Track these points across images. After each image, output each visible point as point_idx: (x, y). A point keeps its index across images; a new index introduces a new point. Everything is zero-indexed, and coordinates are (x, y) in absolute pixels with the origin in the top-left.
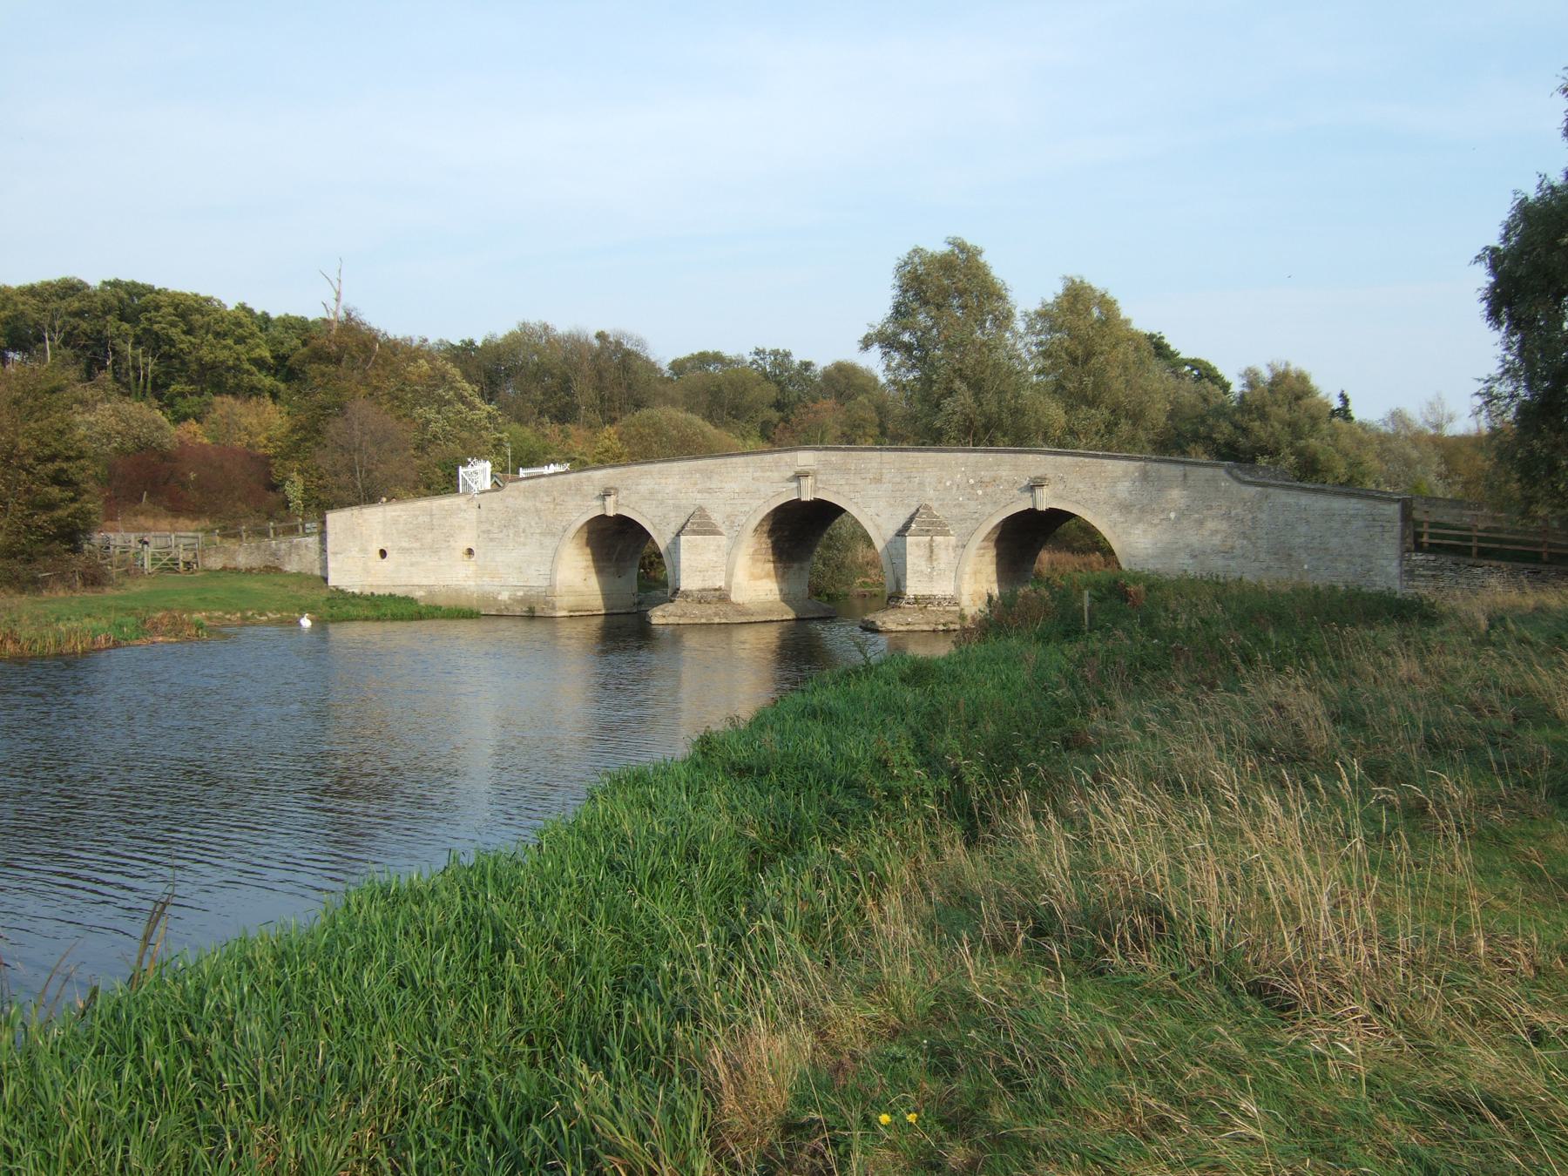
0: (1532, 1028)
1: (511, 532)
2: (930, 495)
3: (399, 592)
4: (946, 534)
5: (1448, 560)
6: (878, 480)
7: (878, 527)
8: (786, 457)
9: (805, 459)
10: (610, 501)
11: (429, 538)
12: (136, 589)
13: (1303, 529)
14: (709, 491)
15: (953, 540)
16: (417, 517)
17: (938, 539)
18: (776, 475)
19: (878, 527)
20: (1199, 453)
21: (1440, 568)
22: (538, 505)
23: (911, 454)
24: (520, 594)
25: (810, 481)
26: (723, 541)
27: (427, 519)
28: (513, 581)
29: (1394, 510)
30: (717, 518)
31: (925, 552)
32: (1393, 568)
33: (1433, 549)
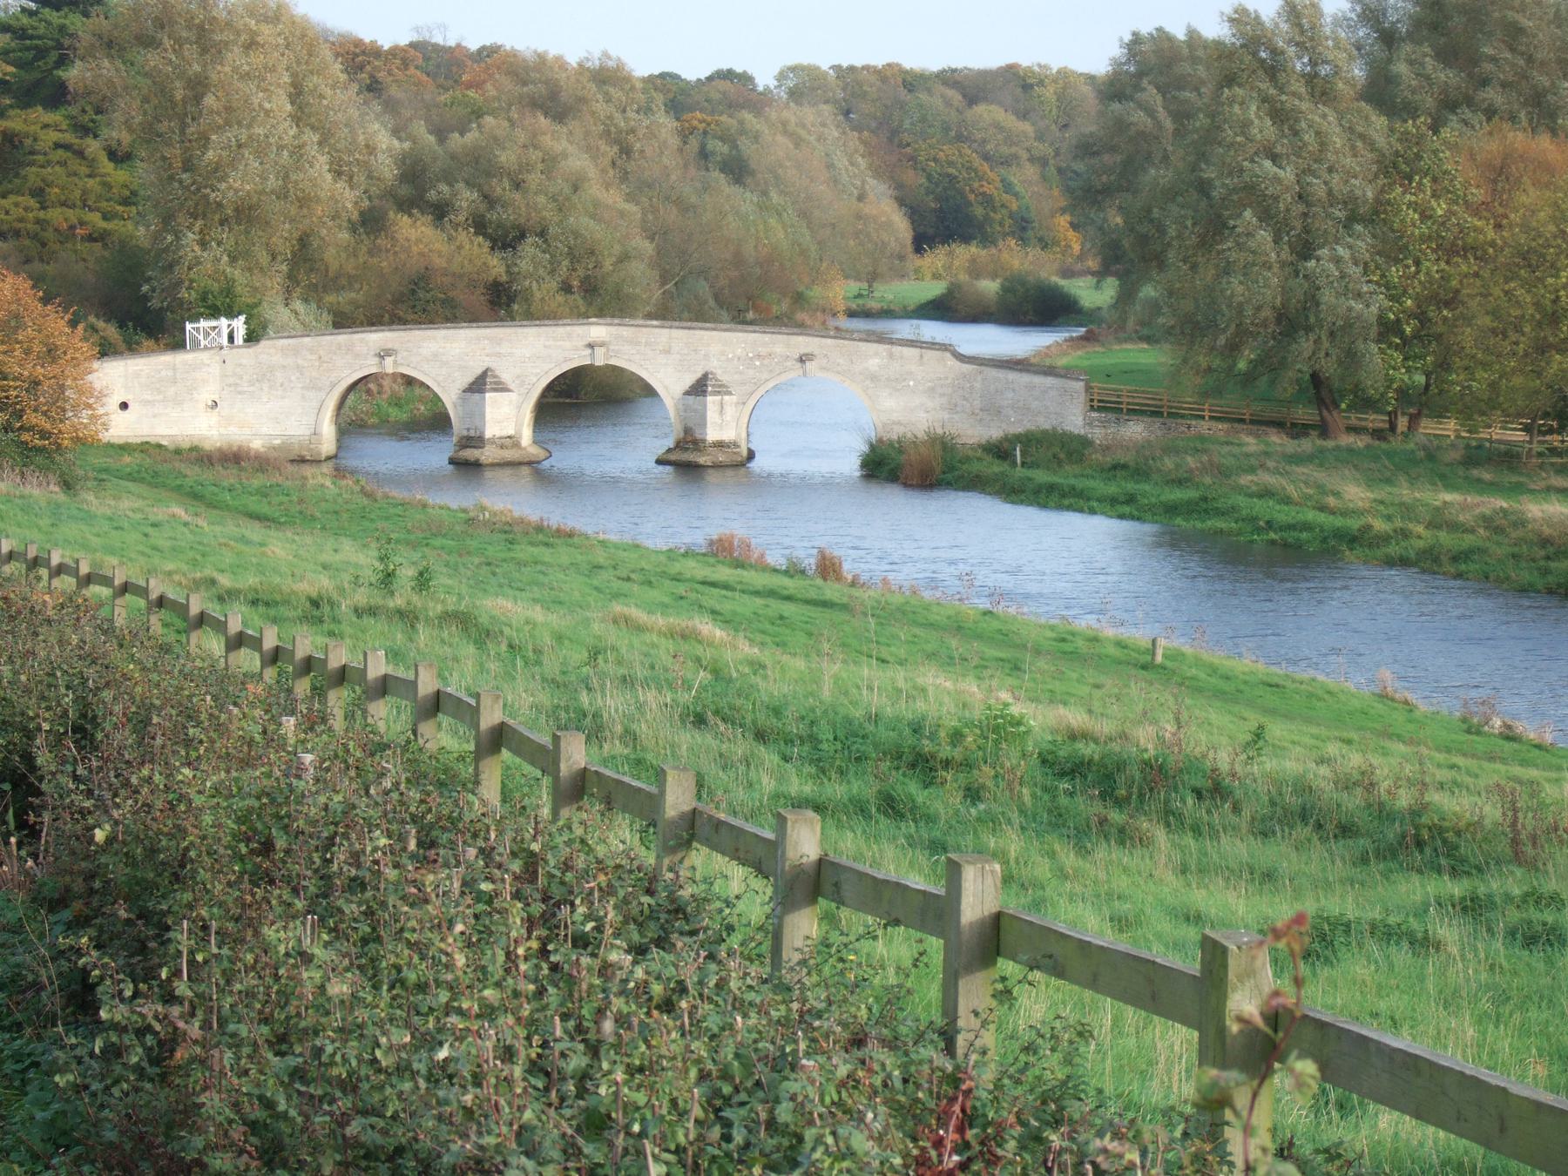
0: (303, 241)
1: (265, 386)
2: (715, 366)
3: (153, 440)
4: (730, 393)
5: (1111, 416)
6: (667, 352)
7: (666, 388)
8: (579, 330)
9: (598, 331)
10: (389, 361)
11: (171, 391)
12: (538, 614)
13: (1011, 395)
14: (499, 355)
15: (734, 398)
16: (159, 372)
17: (726, 398)
18: (567, 344)
19: (666, 388)
20: (1303, 832)
21: (1108, 421)
22: (300, 362)
23: (698, 332)
24: (277, 442)
25: (603, 350)
26: (513, 396)
27: (170, 373)
28: (265, 430)
29: (1080, 386)
30: (506, 377)
31: (717, 408)
32: (1079, 421)
33: (1099, 409)
